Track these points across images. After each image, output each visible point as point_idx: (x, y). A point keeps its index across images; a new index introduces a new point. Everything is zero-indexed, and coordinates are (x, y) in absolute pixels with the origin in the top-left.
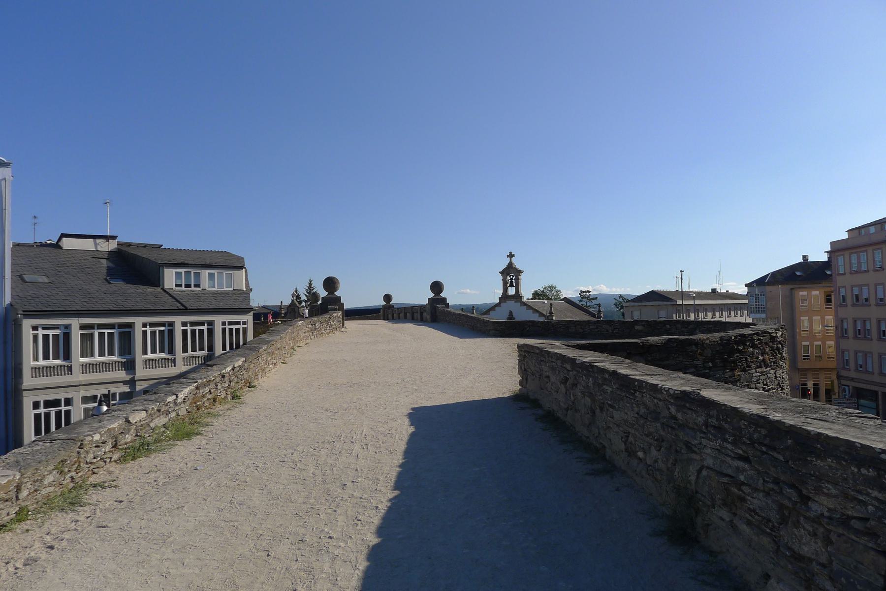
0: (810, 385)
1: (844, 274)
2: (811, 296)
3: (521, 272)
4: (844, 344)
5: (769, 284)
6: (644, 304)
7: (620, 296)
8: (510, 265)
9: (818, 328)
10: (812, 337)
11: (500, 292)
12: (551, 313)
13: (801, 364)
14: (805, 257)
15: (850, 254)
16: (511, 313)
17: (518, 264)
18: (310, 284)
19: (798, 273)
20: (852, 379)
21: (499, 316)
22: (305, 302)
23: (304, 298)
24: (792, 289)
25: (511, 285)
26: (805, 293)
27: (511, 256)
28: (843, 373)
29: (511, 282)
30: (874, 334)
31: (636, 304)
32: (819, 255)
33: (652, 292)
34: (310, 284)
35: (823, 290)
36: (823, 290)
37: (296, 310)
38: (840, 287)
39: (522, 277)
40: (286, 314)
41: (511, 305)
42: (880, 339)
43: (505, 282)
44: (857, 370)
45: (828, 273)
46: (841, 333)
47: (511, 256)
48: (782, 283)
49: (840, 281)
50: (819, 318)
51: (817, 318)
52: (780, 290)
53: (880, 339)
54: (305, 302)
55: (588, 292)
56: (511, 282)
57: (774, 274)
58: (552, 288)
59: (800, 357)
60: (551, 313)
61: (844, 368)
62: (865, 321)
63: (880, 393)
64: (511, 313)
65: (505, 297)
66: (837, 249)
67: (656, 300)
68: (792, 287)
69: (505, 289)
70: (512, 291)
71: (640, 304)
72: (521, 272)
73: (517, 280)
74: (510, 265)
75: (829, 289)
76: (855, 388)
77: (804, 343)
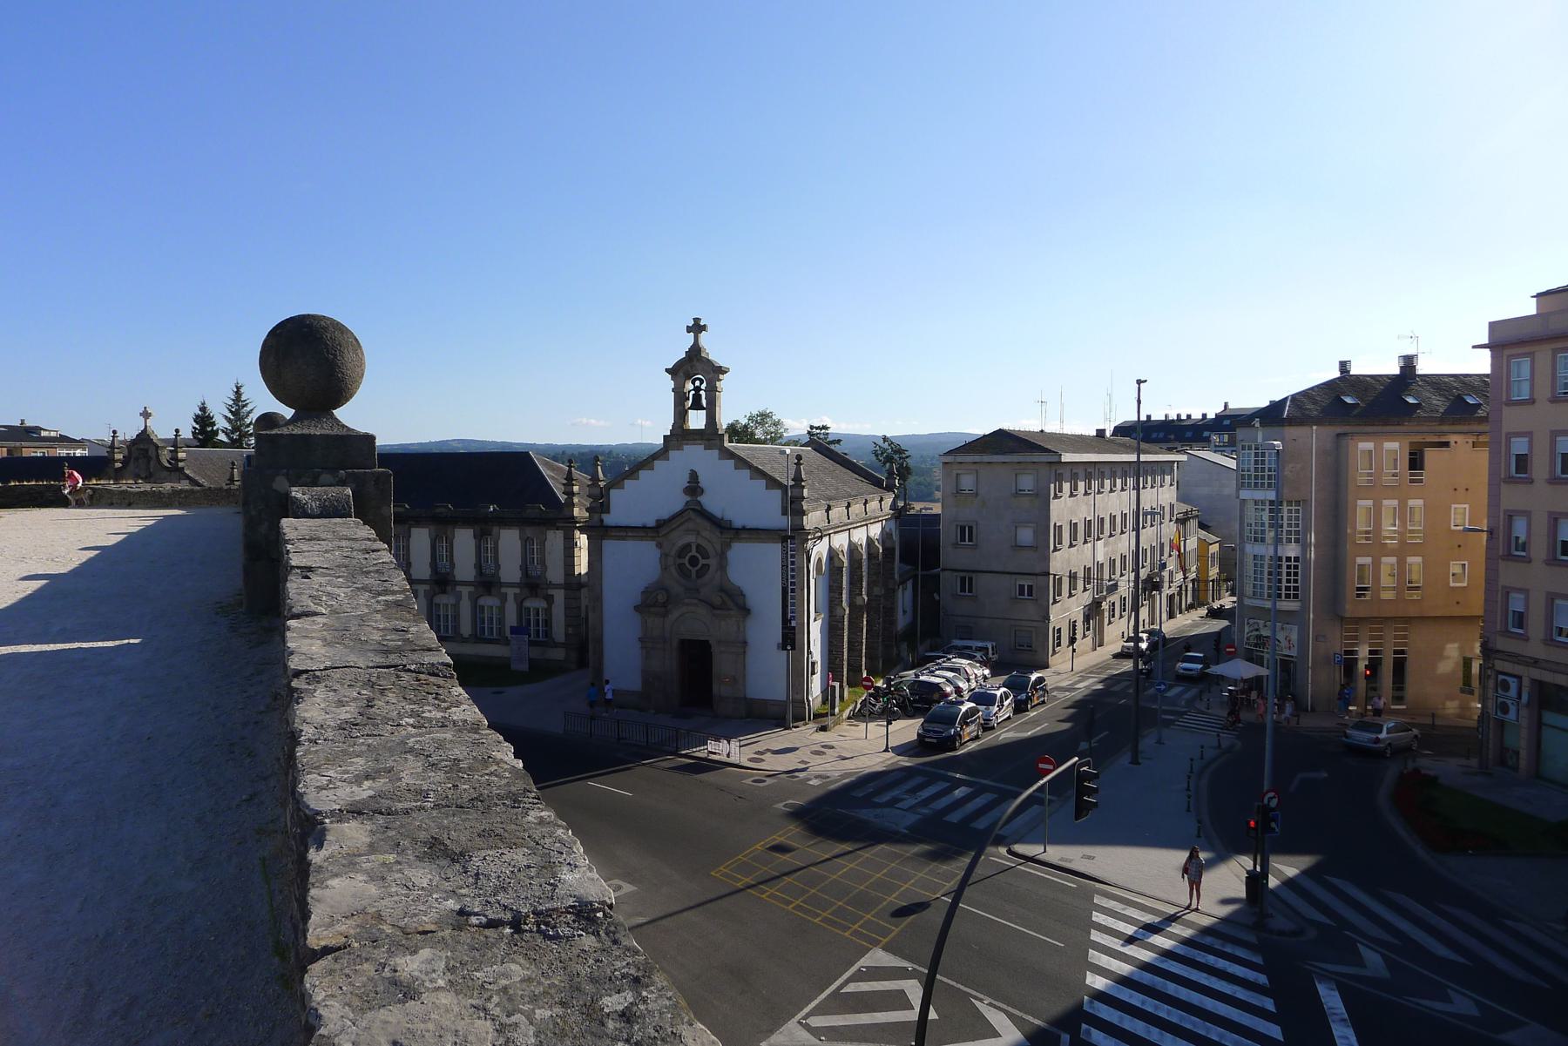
0: (1363, 652)
1: (1531, 401)
2: (1375, 454)
3: (721, 371)
4: (1510, 574)
5: (1291, 421)
6: (986, 458)
7: (885, 439)
8: (695, 353)
9: (1389, 527)
10: (1377, 547)
11: (666, 425)
12: (798, 479)
13: (1351, 608)
14: (1344, 366)
15: (1555, 352)
16: (694, 476)
17: (714, 350)
18: (238, 393)
19: (1349, 400)
20: (1535, 663)
21: (663, 531)
22: (225, 432)
23: (221, 423)
24: (1338, 435)
25: (697, 405)
26: (1369, 445)
27: (697, 328)
28: (1501, 644)
29: (697, 398)
30: (1539, 550)
31: (969, 458)
32: (1458, 354)
33: (1001, 435)
34: (238, 393)
35: (1407, 441)
36: (1407, 441)
37: (152, 452)
38: (1509, 436)
39: (724, 383)
40: (125, 461)
41: (695, 457)
42: (1552, 561)
43: (680, 397)
44: (1549, 641)
45: (1411, 400)
46: (1504, 546)
47: (697, 328)
48: (1318, 422)
49: (1512, 419)
50: (1395, 503)
51: (1390, 503)
52: (1314, 437)
53: (1552, 561)
54: (225, 432)
55: (825, 428)
56: (697, 398)
57: (1298, 399)
58: (764, 417)
59: (1350, 593)
60: (798, 479)
61: (1506, 633)
62: (1556, 520)
63: (1526, 682)
64: (694, 476)
65: (679, 435)
66: (1506, 340)
67: (1012, 451)
68: (1339, 430)
69: (681, 415)
70: (697, 420)
71: (977, 458)
72: (721, 371)
73: (712, 391)
74: (695, 353)
75: (1418, 439)
76: (1539, 685)
77: (1360, 560)
